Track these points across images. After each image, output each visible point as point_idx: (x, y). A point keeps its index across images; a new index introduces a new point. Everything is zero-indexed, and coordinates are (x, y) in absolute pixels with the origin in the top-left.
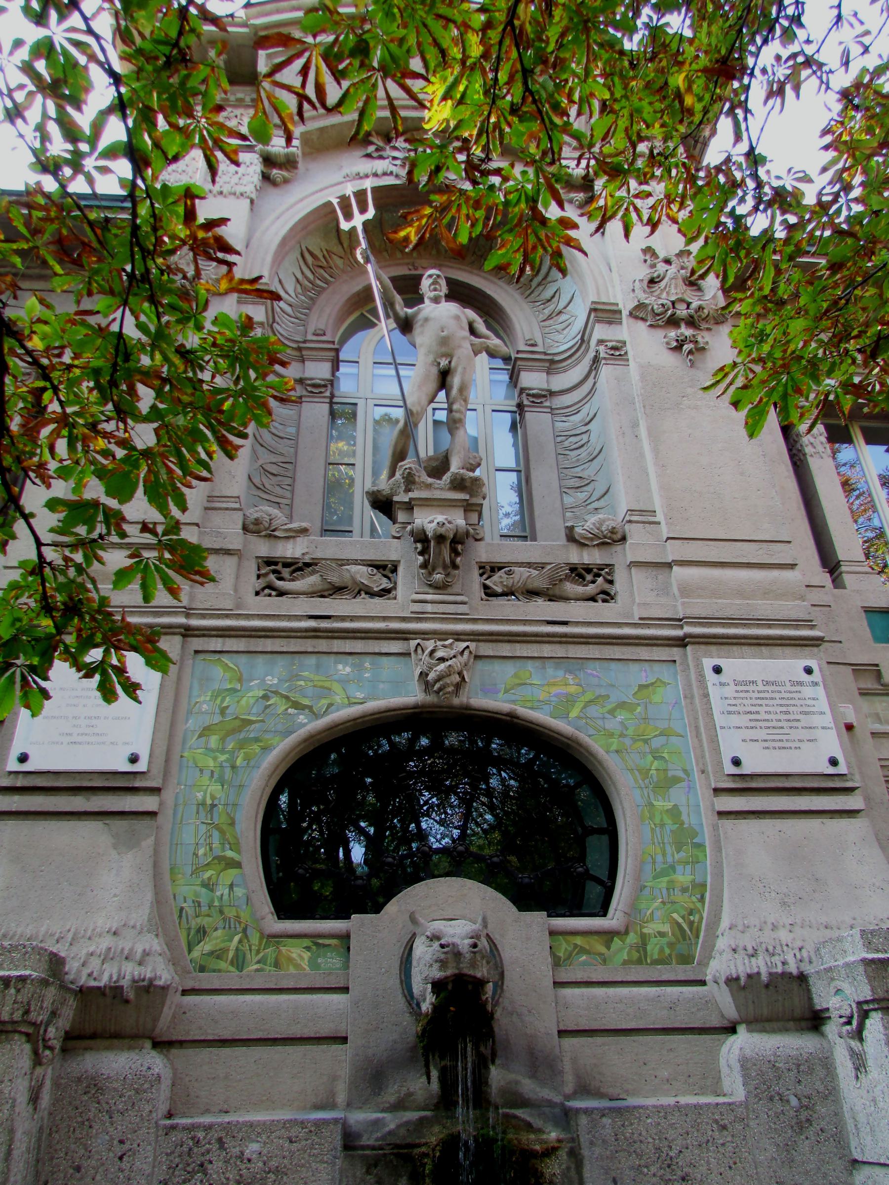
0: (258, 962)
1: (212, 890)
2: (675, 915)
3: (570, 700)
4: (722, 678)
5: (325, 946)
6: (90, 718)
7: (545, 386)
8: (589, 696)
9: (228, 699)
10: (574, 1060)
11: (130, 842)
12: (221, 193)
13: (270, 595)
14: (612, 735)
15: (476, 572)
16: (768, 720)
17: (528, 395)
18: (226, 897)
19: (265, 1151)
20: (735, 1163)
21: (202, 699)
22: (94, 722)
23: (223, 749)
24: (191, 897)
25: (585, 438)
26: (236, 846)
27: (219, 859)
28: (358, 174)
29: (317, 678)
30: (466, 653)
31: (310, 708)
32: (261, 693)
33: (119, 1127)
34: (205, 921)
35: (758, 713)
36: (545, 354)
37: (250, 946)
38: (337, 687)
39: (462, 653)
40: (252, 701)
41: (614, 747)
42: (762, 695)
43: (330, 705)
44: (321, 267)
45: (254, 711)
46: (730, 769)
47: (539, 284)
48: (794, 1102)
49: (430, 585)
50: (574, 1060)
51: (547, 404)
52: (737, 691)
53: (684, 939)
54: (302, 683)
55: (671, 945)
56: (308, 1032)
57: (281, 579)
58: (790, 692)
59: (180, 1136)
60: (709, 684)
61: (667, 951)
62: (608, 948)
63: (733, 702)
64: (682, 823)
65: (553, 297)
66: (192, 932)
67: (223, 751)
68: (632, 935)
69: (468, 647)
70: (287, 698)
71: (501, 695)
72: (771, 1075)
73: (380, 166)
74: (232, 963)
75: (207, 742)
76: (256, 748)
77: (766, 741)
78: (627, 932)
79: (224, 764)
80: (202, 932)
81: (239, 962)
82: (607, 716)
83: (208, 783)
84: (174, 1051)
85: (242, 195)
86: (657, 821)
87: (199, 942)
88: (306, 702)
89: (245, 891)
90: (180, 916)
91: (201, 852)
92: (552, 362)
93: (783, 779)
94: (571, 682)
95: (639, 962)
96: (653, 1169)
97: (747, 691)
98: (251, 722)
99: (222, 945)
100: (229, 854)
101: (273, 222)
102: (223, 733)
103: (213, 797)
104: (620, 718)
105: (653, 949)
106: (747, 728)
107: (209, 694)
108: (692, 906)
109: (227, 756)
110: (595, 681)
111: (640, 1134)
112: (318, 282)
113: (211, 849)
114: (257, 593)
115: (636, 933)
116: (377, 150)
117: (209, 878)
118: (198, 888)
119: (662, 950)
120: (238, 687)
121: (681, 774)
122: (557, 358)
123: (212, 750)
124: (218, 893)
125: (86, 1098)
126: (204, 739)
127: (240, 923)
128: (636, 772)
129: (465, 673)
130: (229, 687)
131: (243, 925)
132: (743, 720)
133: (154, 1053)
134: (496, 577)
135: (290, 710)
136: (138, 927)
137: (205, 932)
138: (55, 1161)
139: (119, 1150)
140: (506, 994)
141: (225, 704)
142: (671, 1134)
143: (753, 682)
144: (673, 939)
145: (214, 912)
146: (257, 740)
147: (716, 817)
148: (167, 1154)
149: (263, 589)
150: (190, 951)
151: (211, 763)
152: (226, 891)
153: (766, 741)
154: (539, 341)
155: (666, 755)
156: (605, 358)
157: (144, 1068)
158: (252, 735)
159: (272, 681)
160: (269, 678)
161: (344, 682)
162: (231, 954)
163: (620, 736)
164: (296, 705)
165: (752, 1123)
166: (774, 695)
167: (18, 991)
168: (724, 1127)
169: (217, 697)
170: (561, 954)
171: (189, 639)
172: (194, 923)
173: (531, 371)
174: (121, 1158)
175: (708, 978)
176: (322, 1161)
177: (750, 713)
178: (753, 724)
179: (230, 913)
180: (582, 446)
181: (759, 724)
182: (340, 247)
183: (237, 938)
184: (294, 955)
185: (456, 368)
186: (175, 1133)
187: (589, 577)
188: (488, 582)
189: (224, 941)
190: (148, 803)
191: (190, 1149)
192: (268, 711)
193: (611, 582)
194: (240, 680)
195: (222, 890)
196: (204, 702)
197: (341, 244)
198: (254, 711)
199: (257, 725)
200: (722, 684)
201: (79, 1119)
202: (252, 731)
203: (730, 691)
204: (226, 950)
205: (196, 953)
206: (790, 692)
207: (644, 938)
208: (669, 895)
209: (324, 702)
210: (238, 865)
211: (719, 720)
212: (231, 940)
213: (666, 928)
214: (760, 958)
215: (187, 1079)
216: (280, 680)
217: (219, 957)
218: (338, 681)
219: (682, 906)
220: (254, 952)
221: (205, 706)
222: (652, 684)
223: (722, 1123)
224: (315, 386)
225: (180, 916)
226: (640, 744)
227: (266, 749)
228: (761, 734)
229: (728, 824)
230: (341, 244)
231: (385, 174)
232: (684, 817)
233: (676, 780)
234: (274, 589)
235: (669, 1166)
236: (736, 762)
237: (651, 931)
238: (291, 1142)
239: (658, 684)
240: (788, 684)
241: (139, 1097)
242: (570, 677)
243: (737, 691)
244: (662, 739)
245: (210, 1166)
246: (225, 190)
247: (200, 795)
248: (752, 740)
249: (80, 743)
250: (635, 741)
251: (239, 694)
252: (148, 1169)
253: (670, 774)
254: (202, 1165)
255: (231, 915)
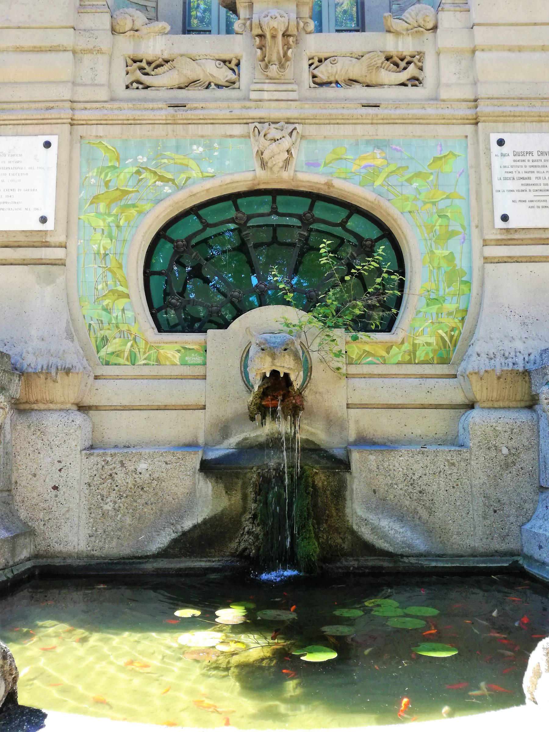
0: (145, 359)
1: (110, 313)
2: (440, 332)
3: (377, 171)
4: (505, 149)
5: (190, 349)
8: (392, 167)
9: (109, 175)
10: (357, 422)
11: (50, 280)
13: (137, 88)
14: (407, 199)
16: (537, 185)
18: (120, 317)
19: (150, 469)
20: (457, 485)
21: (90, 174)
23: (109, 213)
24: (95, 317)
26: (125, 283)
27: (113, 292)
29: (176, 156)
30: (295, 133)
31: (173, 181)
32: (135, 169)
33: (57, 454)
34: (107, 333)
35: (529, 178)
38: (192, 164)
39: (291, 134)
40: (128, 176)
41: (408, 209)
42: (535, 164)
43: (188, 178)
45: (130, 183)
46: (500, 224)
48: (505, 451)
50: (357, 422)
52: (515, 161)
53: (445, 347)
54: (165, 161)
55: (434, 351)
57: (147, 74)
59: (96, 459)
60: (493, 155)
62: (388, 353)
64: (456, 265)
66: (99, 340)
67: (109, 215)
68: (406, 344)
69: (295, 129)
70: (155, 173)
71: (321, 168)
72: (491, 434)
75: (97, 208)
76: (133, 211)
78: (403, 343)
79: (111, 224)
80: (105, 340)
82: (406, 184)
83: (100, 238)
84: (91, 412)
86: (435, 264)
88: (170, 176)
89: (133, 313)
90: (90, 329)
91: (100, 287)
93: (542, 231)
95: (409, 363)
96: (400, 486)
97: (524, 161)
98: (128, 192)
99: (120, 348)
100: (120, 288)
102: (109, 200)
103: (105, 248)
104: (415, 185)
105: (421, 355)
106: (518, 191)
107: (95, 170)
108: (454, 325)
109: (113, 218)
110: (398, 154)
111: (394, 466)
113: (107, 285)
114: (127, 87)
115: (409, 343)
117: (107, 305)
119: (427, 354)
121: (459, 229)
123: (101, 214)
124: (114, 315)
125: (34, 437)
126: (95, 205)
127: (131, 334)
128: (424, 228)
129: (293, 151)
130: (110, 165)
131: (133, 336)
132: (517, 185)
133: (78, 413)
134: (322, 67)
137: (107, 340)
138: (20, 471)
139: (59, 466)
140: (312, 381)
141: (108, 179)
142: (415, 466)
143: (530, 153)
144: (437, 348)
146: (134, 206)
148: (89, 469)
149: (132, 83)
150: (98, 352)
151: (101, 223)
152: (120, 314)
155: (449, 214)
158: (130, 202)
159: (142, 159)
160: (140, 157)
161: (198, 159)
162: (126, 354)
163: (414, 200)
164: (162, 178)
165: (472, 463)
168: (453, 464)
169: (101, 173)
170: (354, 357)
171: (75, 127)
172: (100, 334)
174: (60, 470)
176: (186, 475)
178: (523, 188)
179: (123, 327)
181: (528, 188)
183: (129, 344)
184: (169, 355)
186: (92, 457)
187: (403, 64)
189: (120, 346)
190: (58, 253)
191: (103, 466)
192: (141, 183)
193: (421, 69)
194: (118, 159)
195: (117, 313)
196: (92, 177)
198: (130, 183)
199: (133, 194)
200: (503, 155)
201: (32, 449)
202: (130, 199)
203: (508, 161)
205: (103, 353)
207: (415, 347)
208: (438, 317)
209: (183, 176)
210: (128, 296)
211: (497, 185)
212: (126, 345)
213: (433, 340)
214: (497, 360)
215: (102, 428)
216: (148, 159)
217: (118, 356)
218: (193, 159)
219: (446, 325)
220: (141, 353)
221: (93, 180)
222: (445, 156)
223: (452, 461)
225: (90, 329)
226: (429, 206)
227: (142, 214)
229: (490, 267)
232: (457, 262)
233: (453, 234)
234: (141, 83)
235: (411, 485)
237: (421, 342)
238: (167, 463)
239: (451, 156)
241: (68, 437)
242: (377, 151)
243: (515, 161)
244: (448, 202)
245: (116, 476)
247: (95, 247)
248: (520, 201)
250: (425, 203)
251: (118, 170)
252: (77, 476)
253: (450, 229)
254: (111, 475)
255: (124, 329)
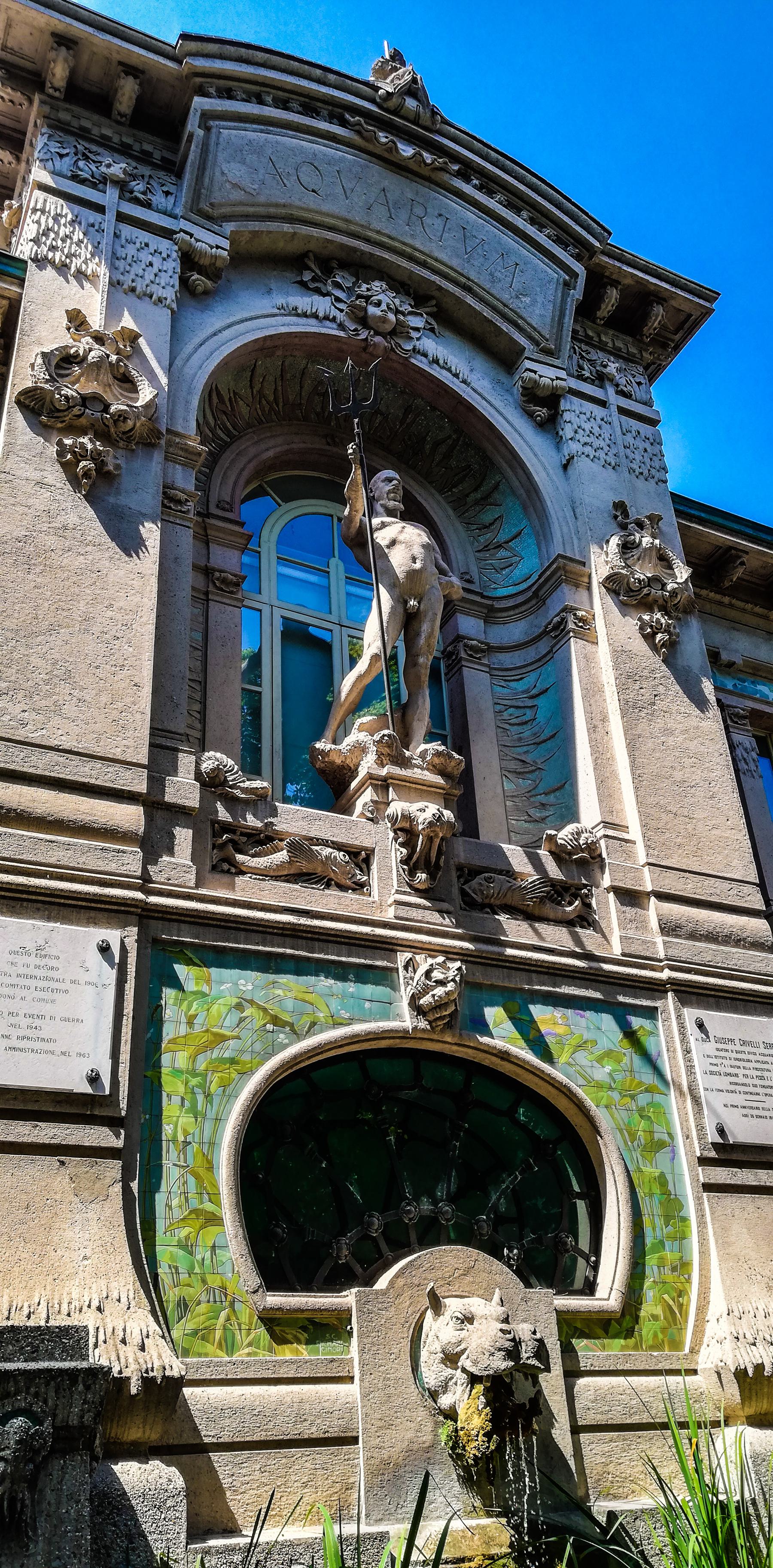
0: (250, 1345)
1: (191, 1253)
2: (666, 1297)
6: (31, 1016)
7: (482, 637)
9: (195, 1006)
12: (133, 290)
15: (454, 874)
17: (466, 645)
18: (207, 1262)
22: (37, 1022)
25: (529, 714)
28: (296, 309)
31: (292, 1025)
32: (235, 1001)
35: (736, 1075)
36: (483, 596)
37: (239, 1325)
40: (224, 1010)
42: (739, 1056)
44: (225, 413)
45: (227, 1023)
47: (477, 502)
49: (411, 886)
51: (485, 661)
52: (718, 1050)
54: (279, 992)
56: (313, 1432)
58: (764, 1055)
61: (660, 1336)
63: (714, 1061)
65: (491, 524)
67: (194, 1073)
70: (265, 1010)
73: (322, 305)
74: (220, 1346)
77: (744, 1107)
81: (228, 1344)
82: (595, 1064)
85: (160, 300)
87: (180, 1319)
88: (286, 1017)
92: (491, 609)
94: (560, 1022)
97: (727, 1051)
98: (223, 1038)
101: (196, 350)
103: (186, 1133)
106: (728, 1091)
112: (219, 432)
115: (631, 1315)
116: (314, 280)
117: (187, 1238)
118: (175, 1250)
119: (655, 1336)
120: (206, 989)
121: (666, 1137)
122: (498, 605)
124: (199, 1257)
130: (195, 989)
135: (268, 1025)
136: (124, 1300)
137: (186, 1306)
141: (192, 1012)
143: (732, 1040)
145: (195, 1281)
147: (701, 1189)
152: (208, 1255)
153: (744, 1107)
154: (476, 578)
156: (573, 631)
157: (164, 1480)
158: (226, 1055)
160: (242, 982)
162: (218, 1334)
166: (751, 1057)
167: (87, 1388)
173: (468, 614)
175: (699, 1368)
177: (730, 1074)
178: (733, 1088)
180: (526, 723)
181: (738, 1088)
182: (249, 390)
183: (223, 1315)
185: (426, 612)
188: (466, 887)
192: (243, 1025)
197: (252, 387)
198: (227, 1023)
204: (211, 1329)
206: (764, 1055)
216: (255, 987)
224: (224, 581)
226: (628, 1099)
228: (739, 1099)
230: (252, 387)
231: (326, 318)
233: (660, 1145)
236: (721, 1131)
240: (762, 1046)
243: (718, 1050)
246: (140, 286)
249: (21, 1050)
253: (657, 1136)
